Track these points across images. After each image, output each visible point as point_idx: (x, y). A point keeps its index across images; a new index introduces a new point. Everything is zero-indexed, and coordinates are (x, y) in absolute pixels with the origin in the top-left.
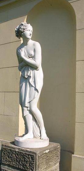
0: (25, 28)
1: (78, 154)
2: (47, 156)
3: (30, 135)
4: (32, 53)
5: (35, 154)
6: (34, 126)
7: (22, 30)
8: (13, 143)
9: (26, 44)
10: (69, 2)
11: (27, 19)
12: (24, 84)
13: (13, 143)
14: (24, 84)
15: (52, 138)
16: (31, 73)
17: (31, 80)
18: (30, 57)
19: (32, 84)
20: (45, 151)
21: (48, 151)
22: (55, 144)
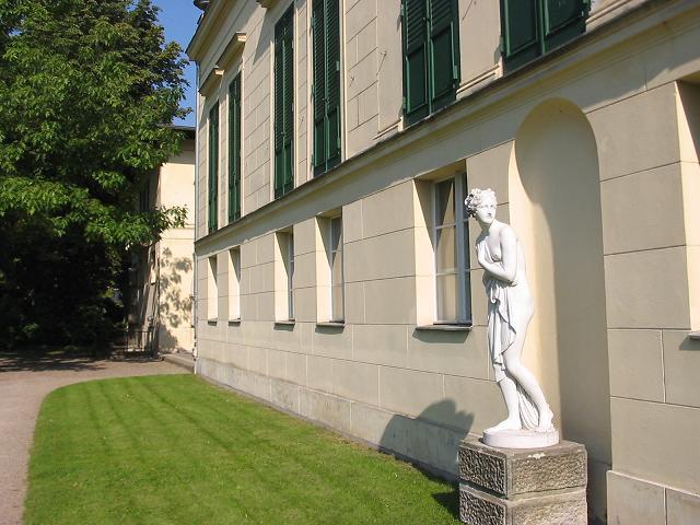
0: (476, 202)
1: (618, 471)
2: (542, 466)
3: (512, 423)
4: (498, 252)
5: (505, 456)
6: (522, 406)
7: (473, 207)
8: (481, 440)
9: (488, 234)
10: (584, 111)
11: (652, 77)
12: (492, 315)
13: (481, 440)
14: (492, 315)
15: (569, 428)
16: (500, 292)
17: (502, 308)
18: (496, 260)
19: (504, 315)
20: (532, 454)
21: (543, 455)
22: (571, 445)
